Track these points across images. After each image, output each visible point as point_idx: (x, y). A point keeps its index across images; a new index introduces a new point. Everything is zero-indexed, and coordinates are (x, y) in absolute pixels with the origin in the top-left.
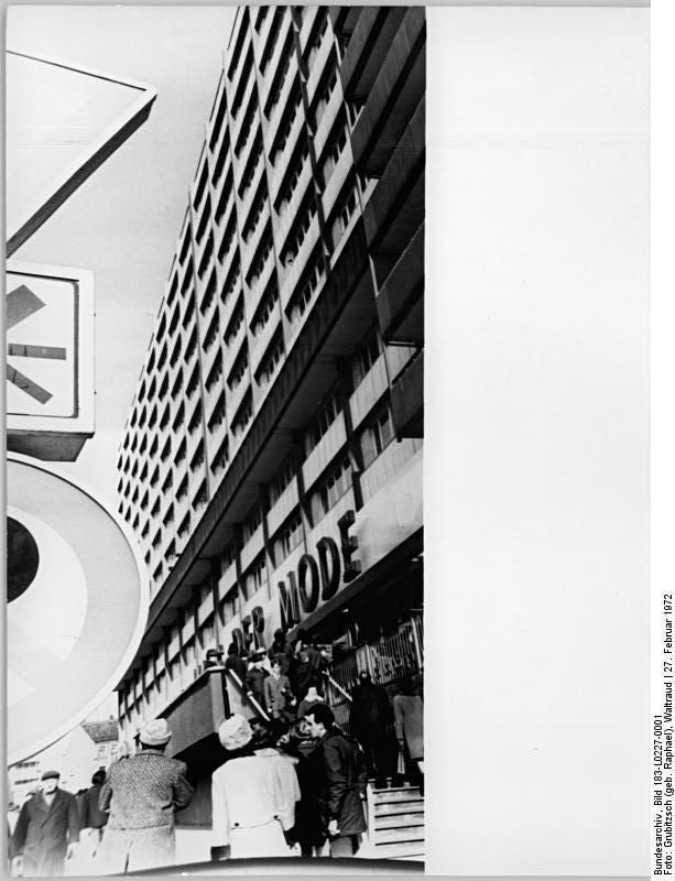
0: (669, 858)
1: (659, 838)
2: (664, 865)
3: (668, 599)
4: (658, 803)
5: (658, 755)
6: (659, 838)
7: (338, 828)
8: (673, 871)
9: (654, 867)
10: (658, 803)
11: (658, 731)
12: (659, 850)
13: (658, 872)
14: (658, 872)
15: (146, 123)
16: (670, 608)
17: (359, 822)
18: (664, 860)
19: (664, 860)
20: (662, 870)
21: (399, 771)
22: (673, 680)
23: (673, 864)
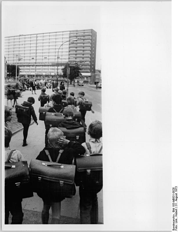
0: (176, 226)
1: (174, 221)
2: (175, 228)
3: (176, 188)
4: (173, 211)
5: (174, 190)
6: (174, 221)
7: (32, 196)
8: (177, 229)
9: (173, 228)
10: (173, 211)
11: (173, 192)
12: (174, 224)
13: (173, 230)
14: (173, 230)
15: (40, 151)
16: (177, 190)
17: (49, 76)
18: (175, 226)
19: (175, 226)
20: (175, 229)
21: (78, 187)
22: (177, 208)
23: (177, 228)
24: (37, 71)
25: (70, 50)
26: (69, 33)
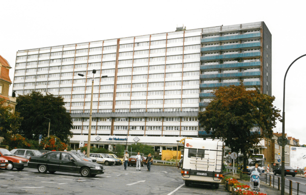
24: (115, 132)
25: (203, 96)
26: (199, 33)
